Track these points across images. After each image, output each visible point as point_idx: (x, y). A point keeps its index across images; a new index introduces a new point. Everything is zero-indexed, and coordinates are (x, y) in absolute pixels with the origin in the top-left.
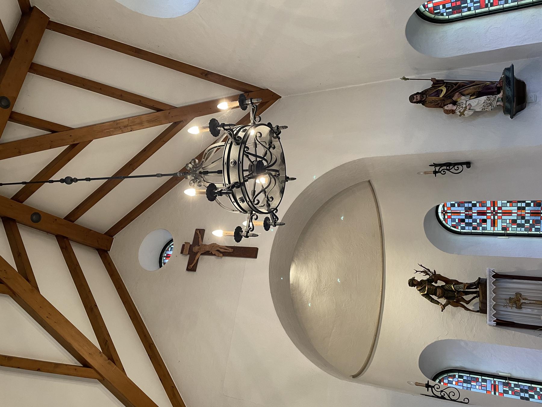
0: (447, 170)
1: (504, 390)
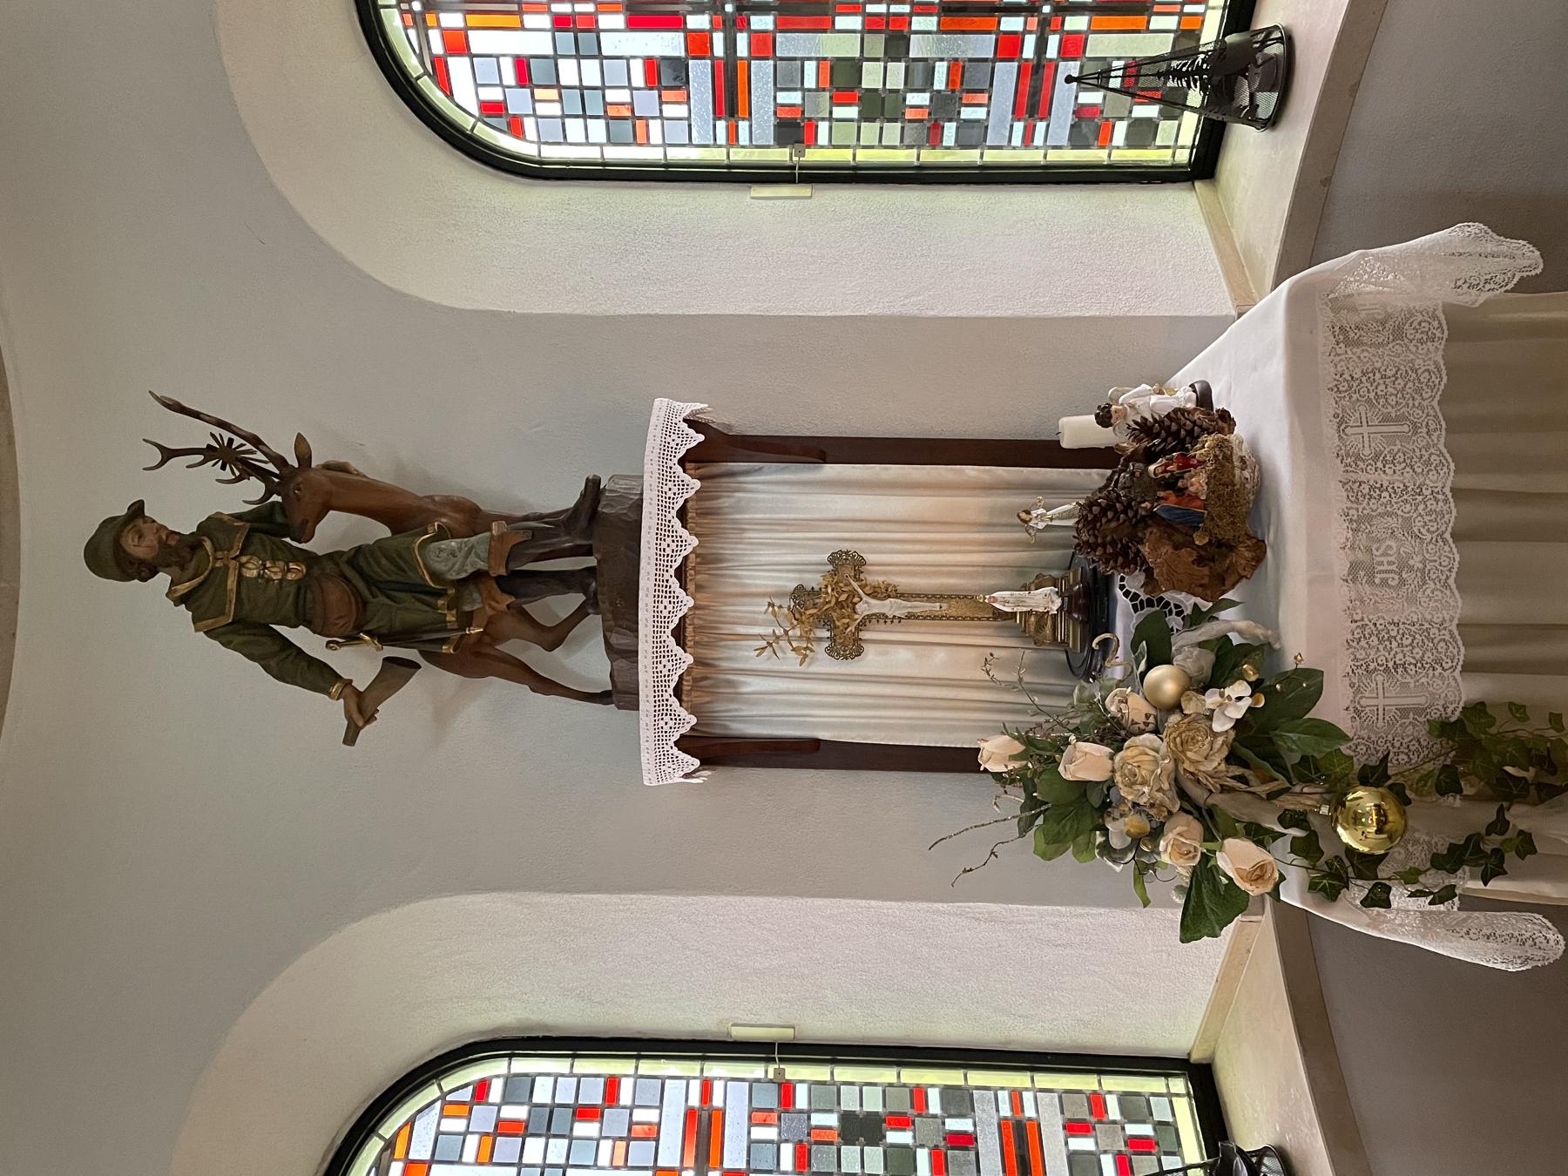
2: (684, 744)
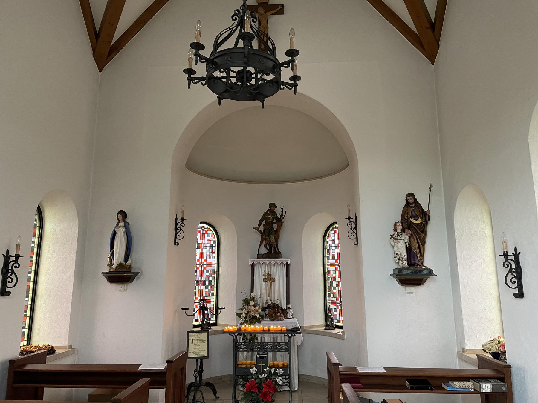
0: (352, 228)
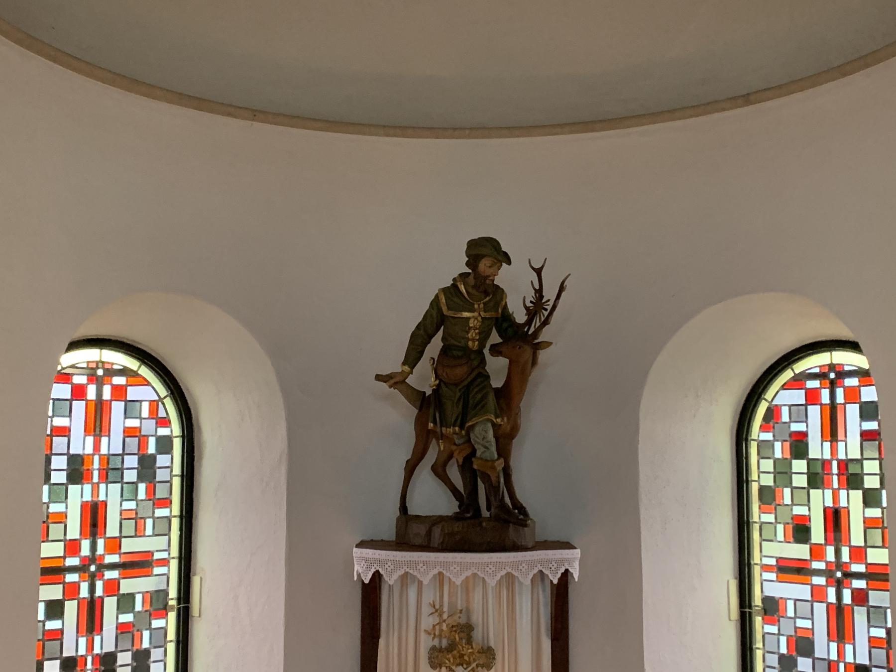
1: (132, 596)
2: (377, 576)
